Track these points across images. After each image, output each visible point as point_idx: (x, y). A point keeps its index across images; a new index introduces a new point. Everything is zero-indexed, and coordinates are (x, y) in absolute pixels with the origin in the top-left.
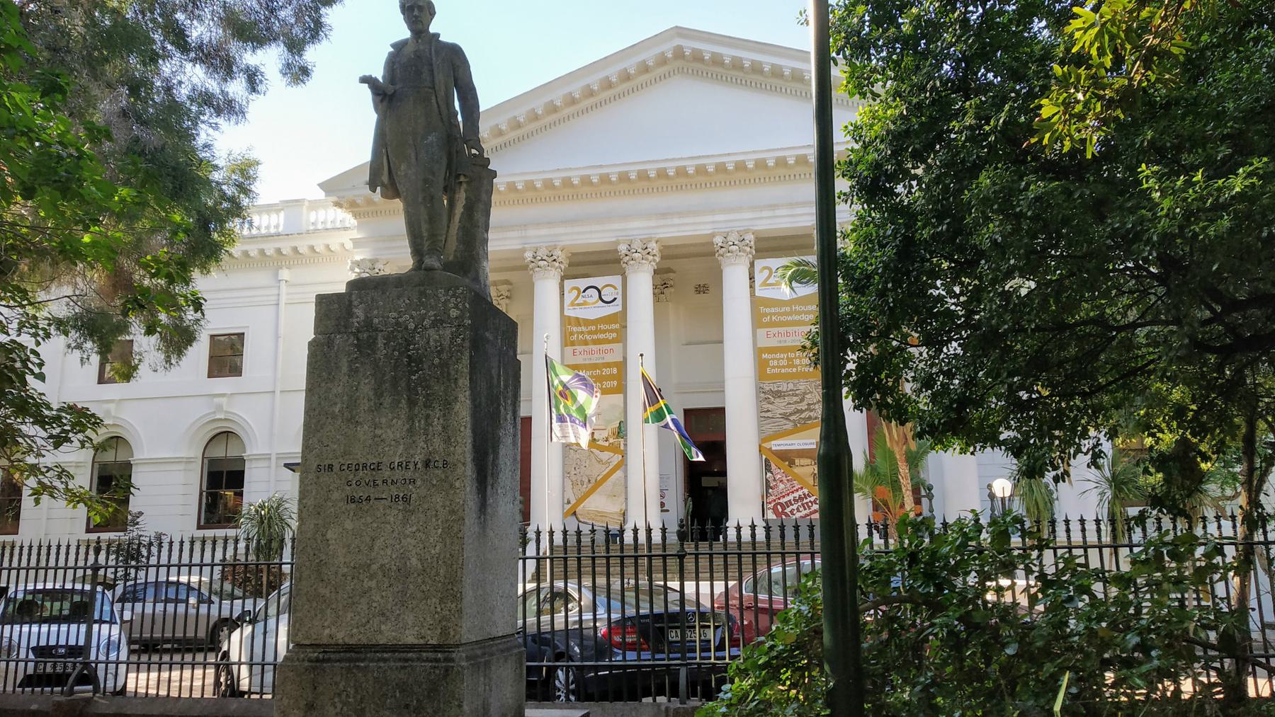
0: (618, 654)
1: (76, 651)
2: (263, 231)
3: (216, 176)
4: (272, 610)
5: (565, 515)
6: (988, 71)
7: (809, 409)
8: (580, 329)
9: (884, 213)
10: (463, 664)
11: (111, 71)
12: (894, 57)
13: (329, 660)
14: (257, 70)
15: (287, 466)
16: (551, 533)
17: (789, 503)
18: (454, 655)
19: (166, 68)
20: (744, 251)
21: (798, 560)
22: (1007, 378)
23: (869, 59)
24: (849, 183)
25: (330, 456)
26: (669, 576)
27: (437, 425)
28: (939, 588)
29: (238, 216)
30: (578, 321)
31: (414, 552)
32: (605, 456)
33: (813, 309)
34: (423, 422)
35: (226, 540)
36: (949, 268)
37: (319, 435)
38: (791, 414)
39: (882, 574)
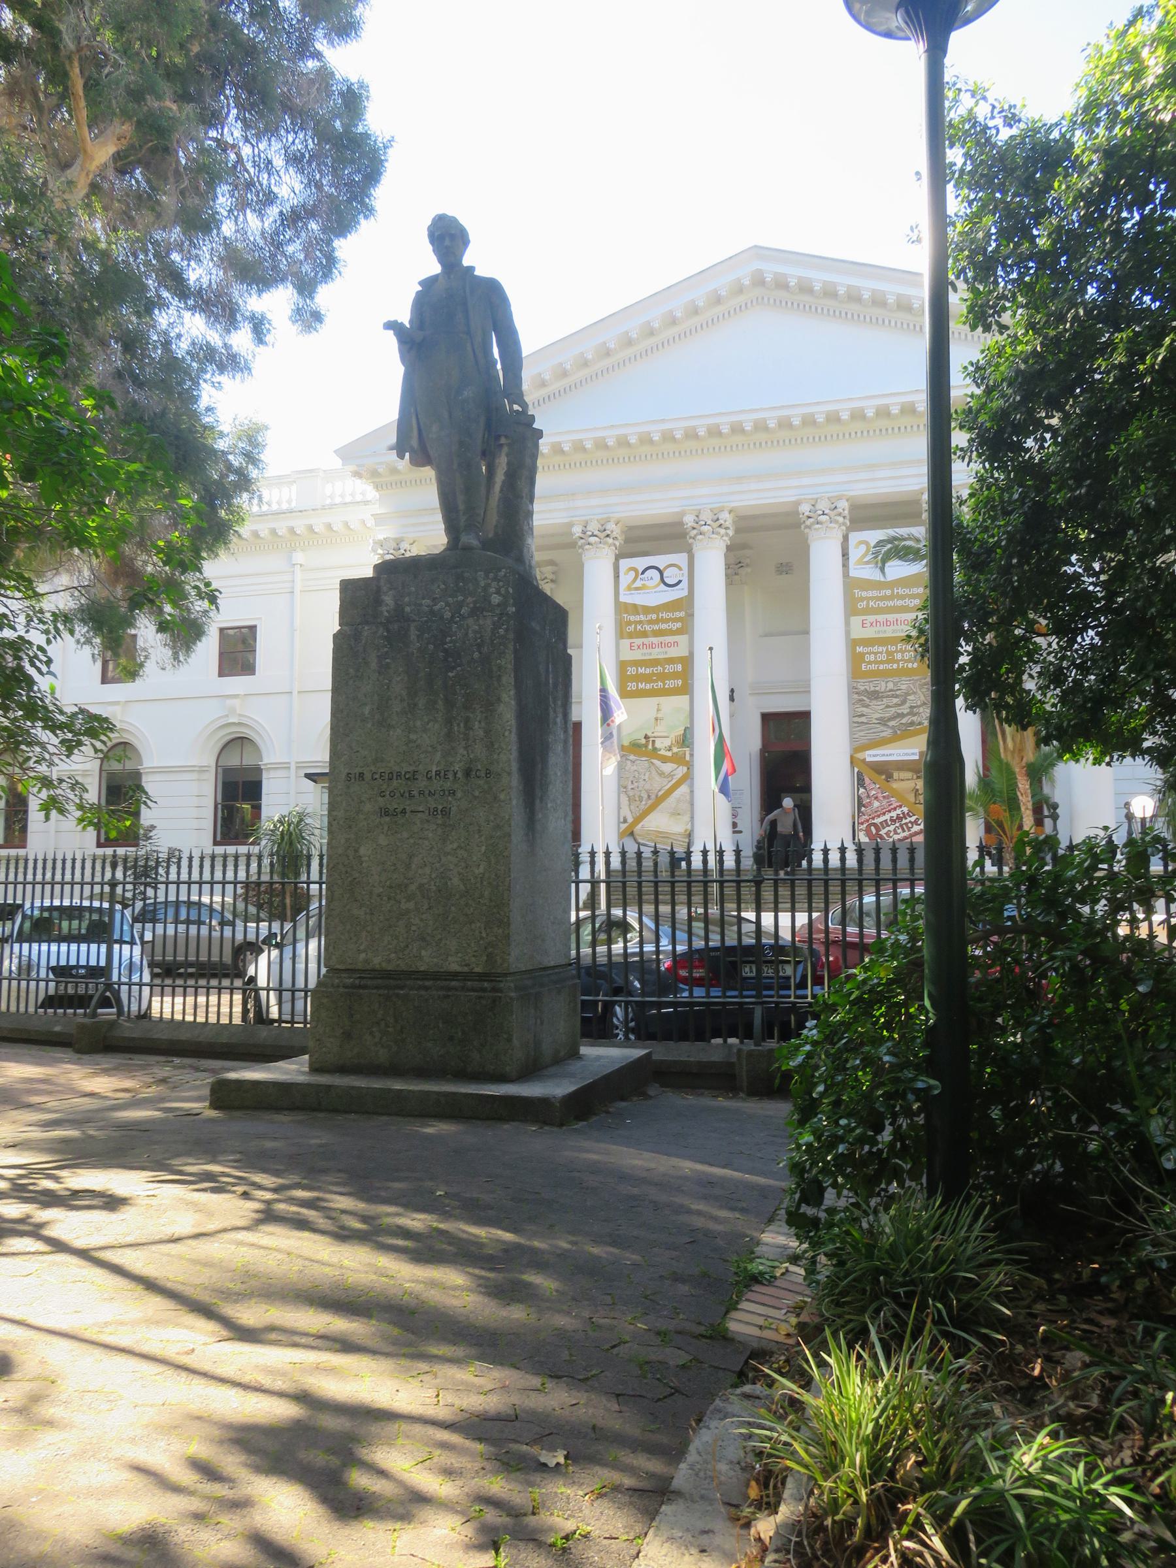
0: (683, 990)
1: (96, 972)
2: (275, 507)
3: (221, 445)
4: (301, 934)
5: (621, 835)
6: (1144, 293)
8: (638, 618)
9: (1010, 472)
10: (512, 994)
11: (104, 325)
12: (1027, 279)
13: (365, 987)
14: (263, 317)
15: (308, 776)
16: (608, 854)
18: (502, 985)
19: (162, 319)
20: (836, 522)
21: (895, 888)
22: (1153, 670)
23: (996, 283)
24: (968, 436)
26: (743, 906)
27: (478, 731)
28: (1062, 916)
29: (247, 490)
30: (635, 609)
32: (668, 767)
33: (920, 593)
35: (249, 856)
36: (1088, 539)
39: (997, 895)
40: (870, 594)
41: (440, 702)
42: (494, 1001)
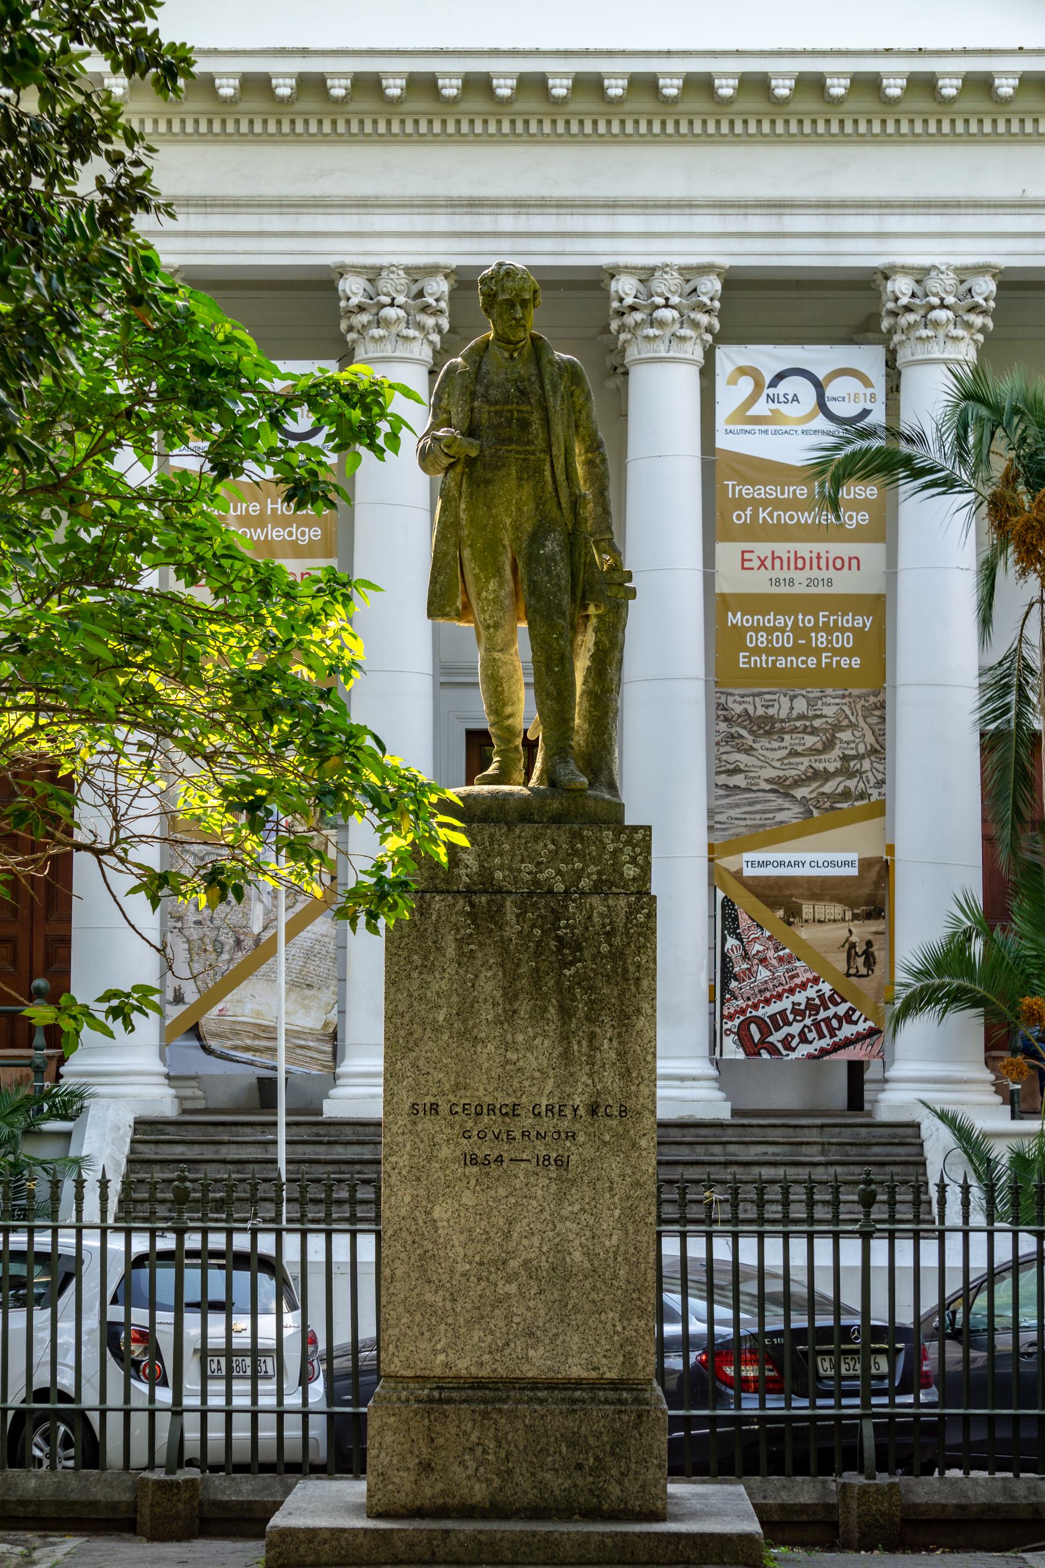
7: (845, 772)
13: (449, 1401)
17: (779, 1020)
25: (434, 1090)
27: (608, 1051)
31: (577, 1242)
34: (584, 1043)
37: (413, 1055)
38: (798, 783)
40: (761, 492)
41: (552, 1011)
42: (640, 1416)
